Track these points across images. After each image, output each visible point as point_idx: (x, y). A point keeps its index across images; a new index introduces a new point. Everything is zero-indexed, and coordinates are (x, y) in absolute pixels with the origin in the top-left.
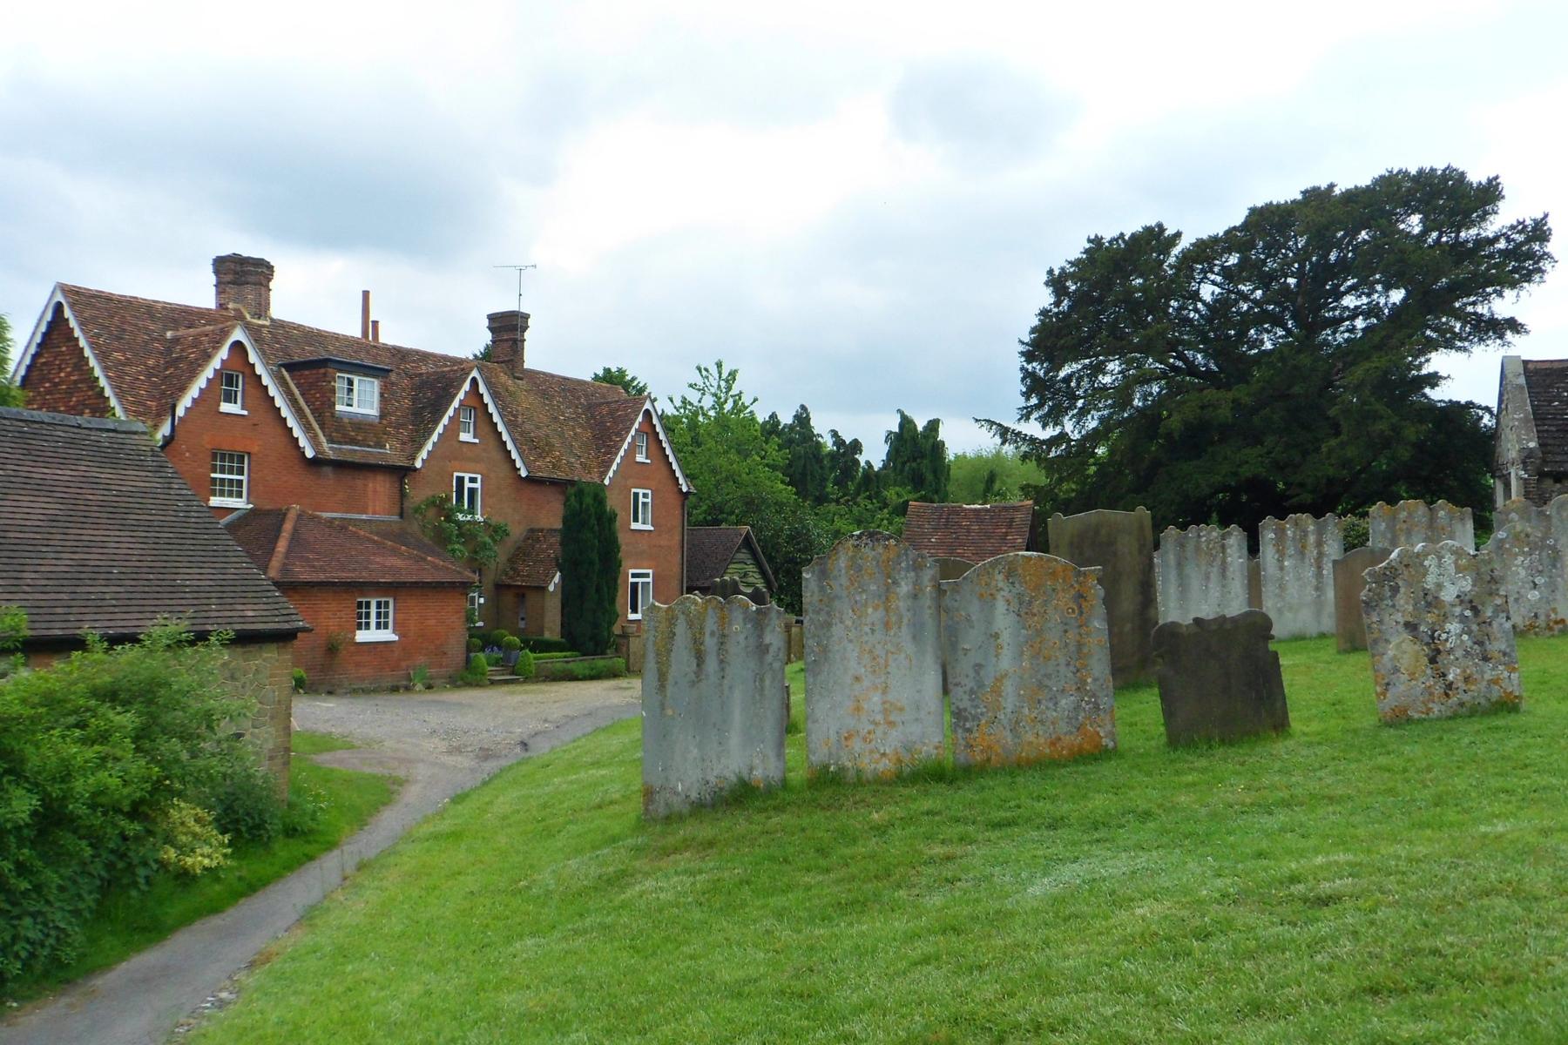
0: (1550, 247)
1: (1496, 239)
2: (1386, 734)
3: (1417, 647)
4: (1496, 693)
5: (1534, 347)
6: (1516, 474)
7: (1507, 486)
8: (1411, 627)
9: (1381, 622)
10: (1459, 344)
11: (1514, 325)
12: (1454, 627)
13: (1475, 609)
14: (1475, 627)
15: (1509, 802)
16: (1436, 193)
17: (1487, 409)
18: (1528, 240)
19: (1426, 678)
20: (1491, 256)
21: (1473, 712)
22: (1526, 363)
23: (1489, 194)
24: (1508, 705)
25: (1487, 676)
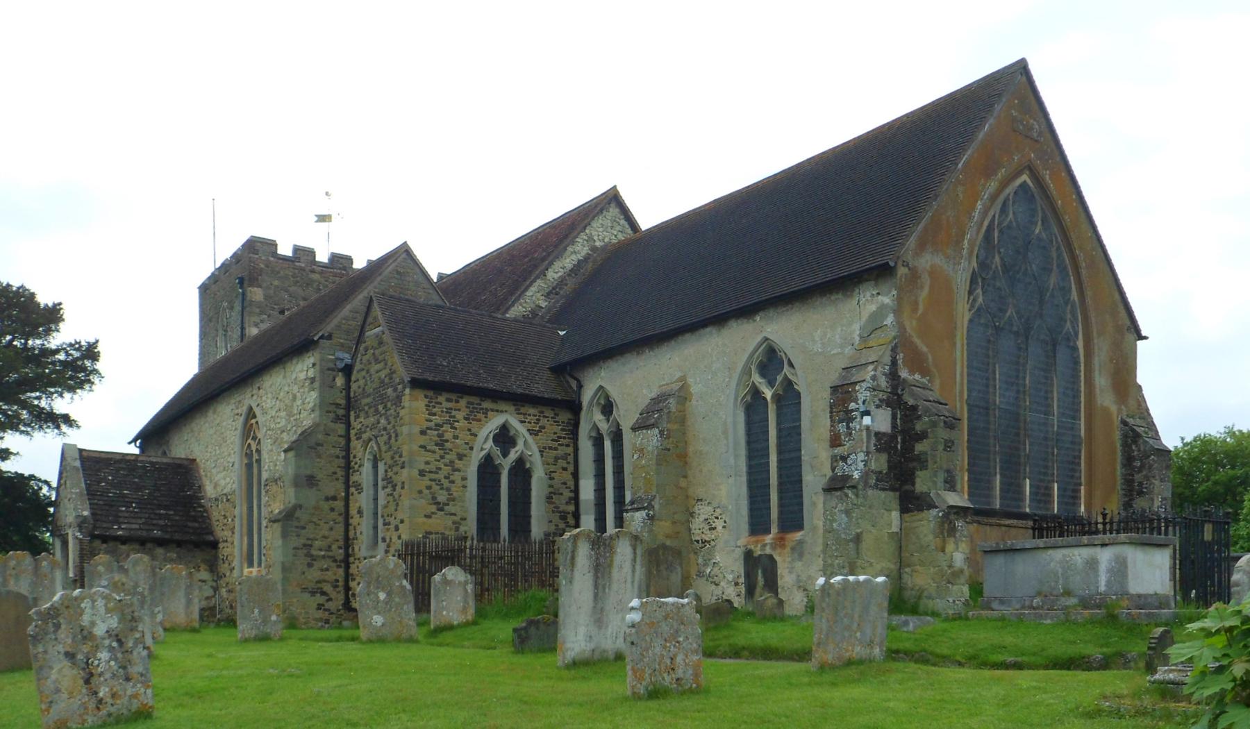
0: (99, 366)
1: (57, 351)
3: (75, 672)
4: (135, 705)
5: (75, 438)
6: (73, 535)
7: (65, 544)
8: (70, 656)
9: (45, 652)
11: (67, 419)
12: (104, 655)
13: (119, 641)
14: (119, 655)
16: (11, 306)
17: (46, 482)
18: (83, 357)
20: (53, 363)
22: (81, 451)
23: (53, 316)
25: (129, 692)
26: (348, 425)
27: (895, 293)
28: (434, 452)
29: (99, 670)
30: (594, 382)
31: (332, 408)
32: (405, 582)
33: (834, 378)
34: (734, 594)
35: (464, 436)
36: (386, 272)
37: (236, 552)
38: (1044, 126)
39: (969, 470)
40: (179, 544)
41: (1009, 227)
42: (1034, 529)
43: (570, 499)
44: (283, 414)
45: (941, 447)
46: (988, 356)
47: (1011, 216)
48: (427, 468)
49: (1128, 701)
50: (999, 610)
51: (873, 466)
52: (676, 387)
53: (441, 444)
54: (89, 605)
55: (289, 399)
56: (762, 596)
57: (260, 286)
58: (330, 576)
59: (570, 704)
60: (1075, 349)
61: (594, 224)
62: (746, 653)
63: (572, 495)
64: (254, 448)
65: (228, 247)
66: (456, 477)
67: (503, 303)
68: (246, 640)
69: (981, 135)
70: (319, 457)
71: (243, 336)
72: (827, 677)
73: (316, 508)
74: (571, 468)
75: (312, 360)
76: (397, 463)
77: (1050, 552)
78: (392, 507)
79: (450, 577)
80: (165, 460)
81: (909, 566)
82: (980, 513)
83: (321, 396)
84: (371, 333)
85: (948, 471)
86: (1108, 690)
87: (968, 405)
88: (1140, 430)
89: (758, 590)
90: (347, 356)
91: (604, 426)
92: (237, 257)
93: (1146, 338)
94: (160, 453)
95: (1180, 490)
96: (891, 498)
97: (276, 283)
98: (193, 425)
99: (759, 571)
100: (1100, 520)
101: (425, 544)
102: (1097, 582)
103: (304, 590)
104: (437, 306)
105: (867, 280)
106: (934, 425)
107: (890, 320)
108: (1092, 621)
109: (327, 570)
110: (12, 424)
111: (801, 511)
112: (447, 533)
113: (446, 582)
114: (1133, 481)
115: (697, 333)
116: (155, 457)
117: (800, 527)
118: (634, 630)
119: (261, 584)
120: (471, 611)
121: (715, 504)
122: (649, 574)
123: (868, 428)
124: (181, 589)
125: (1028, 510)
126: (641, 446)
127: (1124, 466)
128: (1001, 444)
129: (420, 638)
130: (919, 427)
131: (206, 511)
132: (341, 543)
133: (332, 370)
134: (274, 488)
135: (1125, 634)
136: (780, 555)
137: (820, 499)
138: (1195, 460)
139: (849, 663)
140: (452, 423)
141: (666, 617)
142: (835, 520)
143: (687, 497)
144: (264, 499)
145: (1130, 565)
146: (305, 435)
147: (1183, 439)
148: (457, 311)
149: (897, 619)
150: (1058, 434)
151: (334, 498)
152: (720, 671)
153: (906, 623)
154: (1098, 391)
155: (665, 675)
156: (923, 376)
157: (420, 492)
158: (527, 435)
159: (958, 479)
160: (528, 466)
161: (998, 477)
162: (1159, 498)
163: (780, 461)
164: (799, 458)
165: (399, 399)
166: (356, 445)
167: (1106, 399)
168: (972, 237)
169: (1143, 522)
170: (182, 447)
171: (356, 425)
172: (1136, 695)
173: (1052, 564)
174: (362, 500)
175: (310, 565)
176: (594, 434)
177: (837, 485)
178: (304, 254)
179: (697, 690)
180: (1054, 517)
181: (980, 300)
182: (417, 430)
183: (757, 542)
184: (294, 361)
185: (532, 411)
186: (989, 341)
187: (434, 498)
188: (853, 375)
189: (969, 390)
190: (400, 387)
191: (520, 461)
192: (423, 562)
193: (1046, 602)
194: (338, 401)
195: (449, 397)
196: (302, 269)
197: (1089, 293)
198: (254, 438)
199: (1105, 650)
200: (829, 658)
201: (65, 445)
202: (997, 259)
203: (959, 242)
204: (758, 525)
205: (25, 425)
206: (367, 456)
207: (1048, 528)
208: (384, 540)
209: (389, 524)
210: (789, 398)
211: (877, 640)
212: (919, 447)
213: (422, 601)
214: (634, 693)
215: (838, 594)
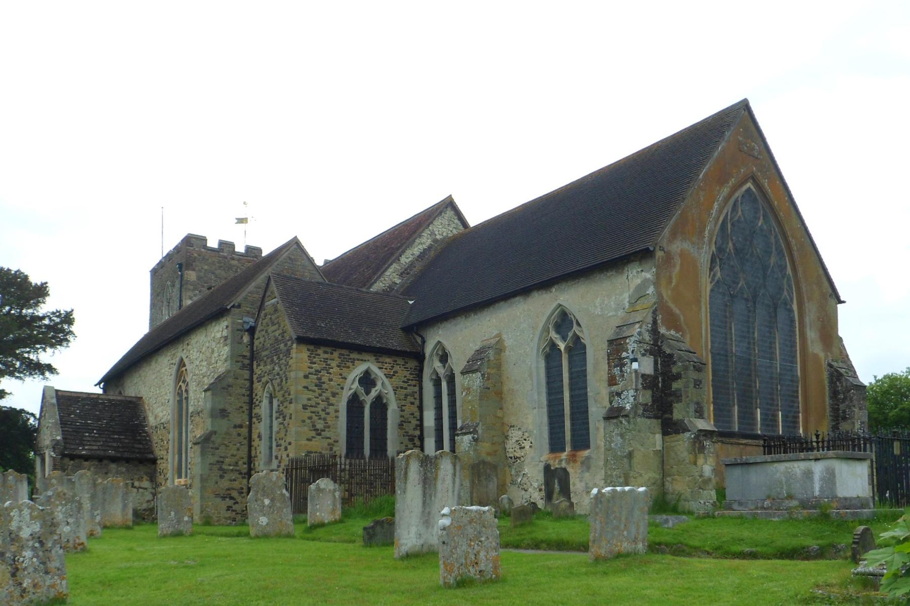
0: (73, 328)
1: (43, 318)
6: (49, 454)
7: (43, 460)
10: (17, 375)
11: (50, 368)
12: (28, 554)
13: (41, 542)
14: (41, 553)
17: (33, 415)
18: (62, 322)
20: (40, 327)
22: (57, 391)
23: (41, 292)
25: (48, 583)
26: (252, 372)
27: (654, 270)
28: (314, 391)
29: (24, 565)
30: (434, 338)
31: (240, 359)
32: (284, 491)
33: (610, 334)
34: (539, 497)
35: (337, 379)
36: (280, 259)
37: (170, 467)
38: (762, 147)
39: (714, 403)
40: (128, 460)
41: (738, 221)
42: (764, 447)
43: (417, 425)
44: (204, 363)
45: (692, 385)
46: (726, 317)
47: (740, 213)
48: (309, 403)
49: (835, 590)
50: (738, 510)
51: (641, 400)
52: (493, 341)
53: (319, 385)
54: (17, 514)
55: (209, 352)
56: (559, 500)
57: (194, 270)
58: (236, 485)
59: (395, 592)
60: (791, 311)
61: (435, 223)
62: (544, 545)
63: (418, 423)
64: (184, 389)
65: (171, 243)
66: (331, 409)
67: (368, 281)
68: (165, 536)
69: (716, 154)
70: (230, 395)
71: (181, 306)
72: (600, 568)
73: (227, 434)
74: (417, 402)
75: (226, 323)
76: (287, 400)
77: (776, 465)
78: (282, 434)
79: (322, 486)
80: (119, 398)
81: (669, 476)
82: (723, 435)
83: (232, 350)
84: (269, 303)
85: (698, 403)
86: (821, 580)
87: (712, 353)
88: (843, 371)
89: (555, 496)
90: (252, 320)
91: (441, 371)
92: (177, 249)
93: (844, 302)
94: (117, 393)
95: (876, 416)
96: (655, 424)
97: (206, 267)
98: (141, 372)
99: (556, 481)
100: (814, 439)
101: (305, 462)
102: (812, 488)
103: (217, 495)
104: (319, 283)
105: (633, 261)
106: (686, 368)
107: (651, 290)
108: (810, 519)
109: (235, 480)
110: (9, 371)
111: (588, 434)
112: (324, 452)
113: (319, 490)
114: (838, 409)
115: (509, 301)
116: (113, 396)
117: (588, 447)
118: (445, 533)
119: (180, 493)
120: (338, 514)
121: (523, 429)
122: (473, 483)
123: (636, 371)
124: (120, 494)
125: (759, 432)
126: (469, 385)
127: (831, 398)
128: (737, 383)
129: (296, 534)
130: (675, 370)
131: (148, 436)
132: (245, 460)
133: (241, 330)
134: (197, 419)
135: (834, 532)
136: (573, 468)
137: (601, 425)
138: (886, 393)
139: (619, 556)
140: (327, 369)
141: (471, 522)
142: (613, 441)
143: (503, 424)
144: (190, 427)
145: (837, 475)
146: (220, 379)
147: (875, 377)
148: (332, 286)
149: (660, 518)
150: (780, 374)
151: (241, 426)
152: (518, 562)
153: (667, 521)
154: (809, 342)
155: (471, 568)
156: (677, 332)
157: (304, 421)
158: (384, 378)
159: (705, 409)
160: (385, 401)
161: (736, 407)
162: (858, 423)
163: (571, 397)
164: (586, 394)
165: (288, 352)
166: (257, 386)
167: (816, 348)
168: (711, 228)
169: (847, 441)
170: (134, 388)
171: (258, 371)
172: (843, 585)
173: (778, 475)
174: (261, 428)
175: (222, 477)
176: (434, 377)
177: (614, 414)
178: (226, 246)
179: (497, 580)
180: (779, 438)
181: (719, 274)
182: (301, 374)
183: (556, 458)
184: (213, 324)
185: (388, 360)
186: (726, 305)
187: (314, 426)
188: (624, 332)
189: (712, 342)
190: (289, 343)
191: (379, 398)
192: (302, 475)
193: (774, 504)
194: (244, 354)
195: (326, 349)
196: (225, 257)
197: (800, 270)
198: (184, 382)
199: (820, 542)
200: (603, 552)
201: (45, 387)
202: (730, 244)
203: (702, 232)
204: (556, 445)
205: (20, 372)
206: (265, 394)
207: (775, 446)
208: (276, 457)
209: (280, 445)
210: (577, 349)
211: (640, 537)
212: (675, 386)
213: (300, 505)
214: (445, 583)
215: (609, 501)
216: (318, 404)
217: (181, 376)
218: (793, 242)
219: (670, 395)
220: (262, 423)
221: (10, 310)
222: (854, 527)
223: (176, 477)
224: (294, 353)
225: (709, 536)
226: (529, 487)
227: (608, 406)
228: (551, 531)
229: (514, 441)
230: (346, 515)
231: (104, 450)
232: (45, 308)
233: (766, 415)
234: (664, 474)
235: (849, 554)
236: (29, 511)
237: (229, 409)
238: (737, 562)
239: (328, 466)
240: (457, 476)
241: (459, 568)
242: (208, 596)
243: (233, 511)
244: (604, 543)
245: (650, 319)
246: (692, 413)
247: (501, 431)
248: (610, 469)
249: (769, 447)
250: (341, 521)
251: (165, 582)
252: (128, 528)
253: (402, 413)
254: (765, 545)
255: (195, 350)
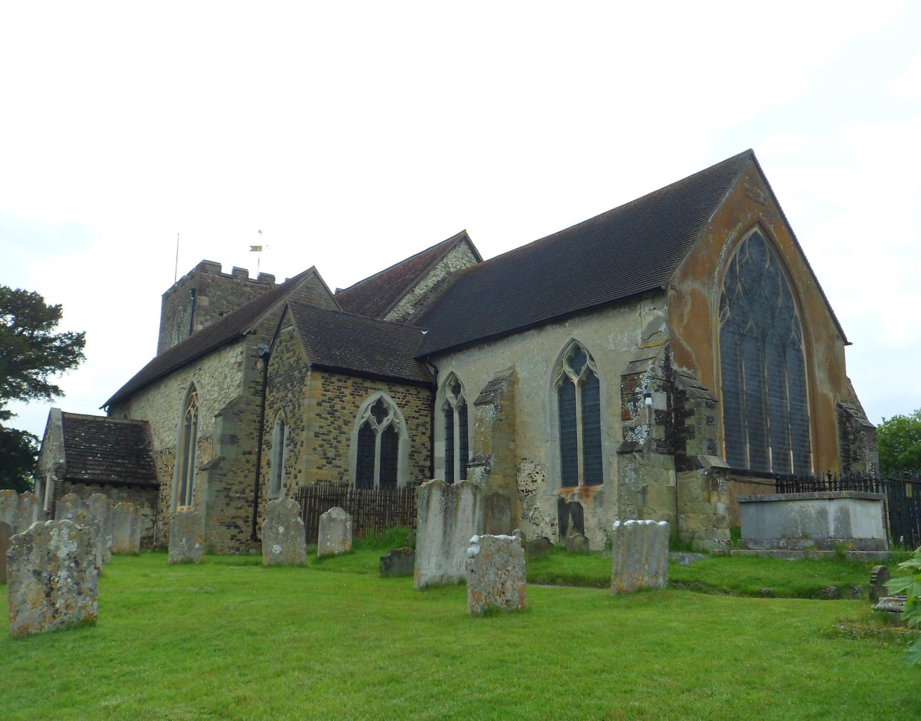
0: (84, 351)
1: (54, 339)
2: (14, 645)
3: (39, 586)
4: (83, 615)
7: (43, 485)
8: (37, 573)
9: (18, 570)
10: (22, 396)
11: (56, 390)
12: (63, 573)
13: (77, 563)
14: (75, 574)
15: (109, 684)
16: (24, 306)
17: (35, 437)
18: (73, 344)
19: (43, 607)
20: (51, 348)
21: (69, 627)
22: (64, 413)
23: (55, 314)
24: (89, 622)
25: (79, 604)
26: (264, 398)
28: (326, 419)
29: (59, 585)
30: (447, 369)
31: (253, 385)
32: (299, 519)
33: (623, 369)
34: (550, 533)
35: (349, 407)
38: (767, 194)
39: (726, 440)
40: (130, 486)
41: (747, 263)
42: (777, 486)
43: (427, 456)
44: (216, 388)
45: (704, 422)
46: (736, 355)
47: (747, 255)
48: (321, 431)
49: (858, 625)
50: (755, 549)
51: (654, 435)
52: (507, 373)
53: (332, 413)
55: (222, 378)
56: (572, 534)
57: (207, 296)
58: (242, 513)
60: (799, 351)
61: (449, 256)
62: (560, 580)
63: (429, 453)
64: (192, 413)
65: (185, 270)
66: (342, 438)
67: (382, 311)
69: (724, 200)
71: (191, 330)
72: (623, 601)
73: (235, 460)
74: (428, 433)
75: (240, 349)
77: (790, 504)
78: (293, 461)
79: (334, 516)
80: (125, 422)
82: (736, 473)
83: (246, 376)
84: (285, 330)
85: (710, 440)
86: (842, 616)
88: (852, 412)
89: (569, 530)
90: (266, 346)
91: (454, 402)
92: (192, 275)
93: (850, 344)
94: (122, 416)
95: (885, 458)
96: (668, 460)
97: (219, 293)
99: (570, 515)
100: (827, 479)
102: (827, 528)
103: (222, 524)
106: (698, 405)
107: (663, 327)
108: (826, 559)
109: (241, 508)
110: (15, 392)
112: (334, 481)
113: (331, 519)
114: (849, 450)
116: (118, 419)
117: (601, 481)
118: (473, 560)
120: (348, 546)
121: (536, 462)
122: (486, 516)
123: (649, 406)
124: (128, 521)
125: (771, 471)
126: (481, 418)
127: (842, 438)
128: (748, 420)
129: (309, 564)
130: (687, 406)
131: (152, 461)
132: (253, 488)
133: (255, 356)
134: (206, 444)
137: (615, 460)
138: (894, 435)
139: (640, 590)
140: (341, 398)
141: (498, 551)
142: (626, 476)
144: (197, 453)
146: (231, 404)
147: (884, 419)
150: (791, 413)
151: (250, 453)
152: (540, 595)
153: (683, 558)
154: (818, 382)
155: (497, 597)
157: (315, 449)
158: (396, 407)
160: (396, 430)
162: (869, 463)
163: (584, 430)
165: (302, 379)
166: (269, 412)
167: (825, 388)
168: (720, 270)
169: (859, 482)
170: (139, 412)
171: (270, 397)
174: (271, 455)
175: (228, 505)
177: (627, 449)
178: (240, 273)
179: (522, 610)
180: (792, 477)
181: (729, 314)
182: (315, 402)
183: (568, 492)
185: (401, 389)
186: (736, 344)
187: (325, 454)
188: (637, 367)
189: (724, 380)
190: (304, 370)
191: (391, 427)
192: (314, 503)
193: (790, 544)
194: (258, 380)
196: (239, 284)
197: (807, 311)
198: (194, 406)
199: (837, 582)
200: (625, 585)
202: (739, 285)
204: (568, 479)
205: (25, 393)
208: (285, 486)
209: (290, 473)
210: (591, 383)
211: (661, 572)
212: (688, 422)
213: (312, 535)
214: (473, 612)
215: (630, 534)
216: (330, 432)
217: (190, 401)
218: (800, 285)
219: (683, 431)
220: (272, 450)
221: (23, 331)
222: (870, 569)
223: (179, 504)
224: (308, 381)
225: (726, 574)
226: (543, 518)
227: (622, 440)
228: (566, 566)
229: (526, 473)
230: (356, 545)
231: (107, 475)
232: (57, 330)
233: (778, 453)
234: (678, 511)
235: (867, 595)
236: (68, 531)
237: (240, 435)
238: (757, 600)
239: (337, 495)
240: (478, 506)
241: (486, 597)
242: (237, 621)
243: (237, 540)
244: (625, 577)
245: (662, 356)
246: (705, 450)
247: (513, 464)
248: (624, 505)
249: (782, 486)
250: (351, 552)
251: (190, 607)
252: (135, 555)
253: (413, 443)
254: (783, 585)
255: (207, 375)
